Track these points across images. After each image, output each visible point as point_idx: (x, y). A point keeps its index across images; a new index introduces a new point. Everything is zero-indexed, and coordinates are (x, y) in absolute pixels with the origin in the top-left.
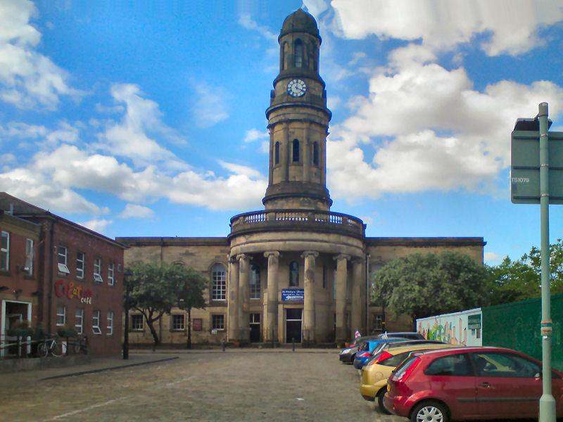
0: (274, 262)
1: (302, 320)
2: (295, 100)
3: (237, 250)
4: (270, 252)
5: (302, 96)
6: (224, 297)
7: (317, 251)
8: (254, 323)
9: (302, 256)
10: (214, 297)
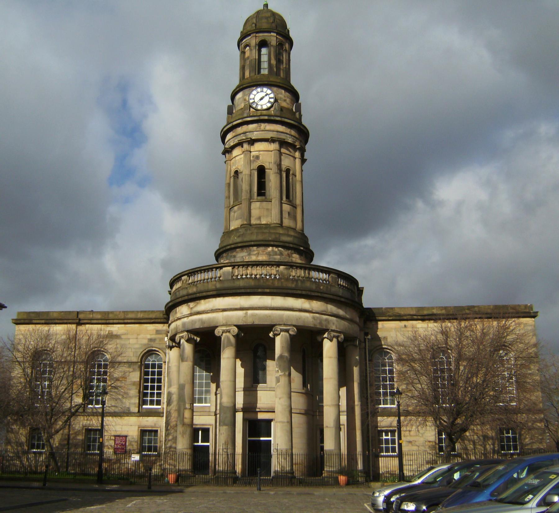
0: (229, 344)
1: (162, 377)
2: (259, 113)
3: (176, 328)
4: (224, 328)
5: (268, 109)
6: (158, 403)
7: (294, 326)
8: (200, 443)
9: (271, 335)
10: (145, 402)
